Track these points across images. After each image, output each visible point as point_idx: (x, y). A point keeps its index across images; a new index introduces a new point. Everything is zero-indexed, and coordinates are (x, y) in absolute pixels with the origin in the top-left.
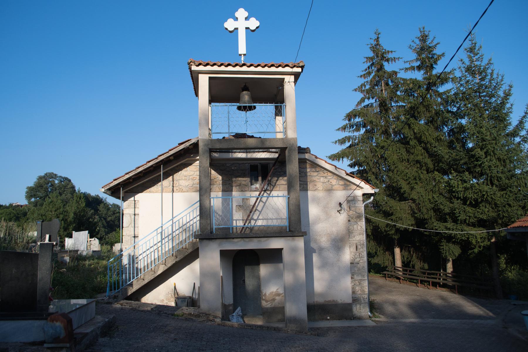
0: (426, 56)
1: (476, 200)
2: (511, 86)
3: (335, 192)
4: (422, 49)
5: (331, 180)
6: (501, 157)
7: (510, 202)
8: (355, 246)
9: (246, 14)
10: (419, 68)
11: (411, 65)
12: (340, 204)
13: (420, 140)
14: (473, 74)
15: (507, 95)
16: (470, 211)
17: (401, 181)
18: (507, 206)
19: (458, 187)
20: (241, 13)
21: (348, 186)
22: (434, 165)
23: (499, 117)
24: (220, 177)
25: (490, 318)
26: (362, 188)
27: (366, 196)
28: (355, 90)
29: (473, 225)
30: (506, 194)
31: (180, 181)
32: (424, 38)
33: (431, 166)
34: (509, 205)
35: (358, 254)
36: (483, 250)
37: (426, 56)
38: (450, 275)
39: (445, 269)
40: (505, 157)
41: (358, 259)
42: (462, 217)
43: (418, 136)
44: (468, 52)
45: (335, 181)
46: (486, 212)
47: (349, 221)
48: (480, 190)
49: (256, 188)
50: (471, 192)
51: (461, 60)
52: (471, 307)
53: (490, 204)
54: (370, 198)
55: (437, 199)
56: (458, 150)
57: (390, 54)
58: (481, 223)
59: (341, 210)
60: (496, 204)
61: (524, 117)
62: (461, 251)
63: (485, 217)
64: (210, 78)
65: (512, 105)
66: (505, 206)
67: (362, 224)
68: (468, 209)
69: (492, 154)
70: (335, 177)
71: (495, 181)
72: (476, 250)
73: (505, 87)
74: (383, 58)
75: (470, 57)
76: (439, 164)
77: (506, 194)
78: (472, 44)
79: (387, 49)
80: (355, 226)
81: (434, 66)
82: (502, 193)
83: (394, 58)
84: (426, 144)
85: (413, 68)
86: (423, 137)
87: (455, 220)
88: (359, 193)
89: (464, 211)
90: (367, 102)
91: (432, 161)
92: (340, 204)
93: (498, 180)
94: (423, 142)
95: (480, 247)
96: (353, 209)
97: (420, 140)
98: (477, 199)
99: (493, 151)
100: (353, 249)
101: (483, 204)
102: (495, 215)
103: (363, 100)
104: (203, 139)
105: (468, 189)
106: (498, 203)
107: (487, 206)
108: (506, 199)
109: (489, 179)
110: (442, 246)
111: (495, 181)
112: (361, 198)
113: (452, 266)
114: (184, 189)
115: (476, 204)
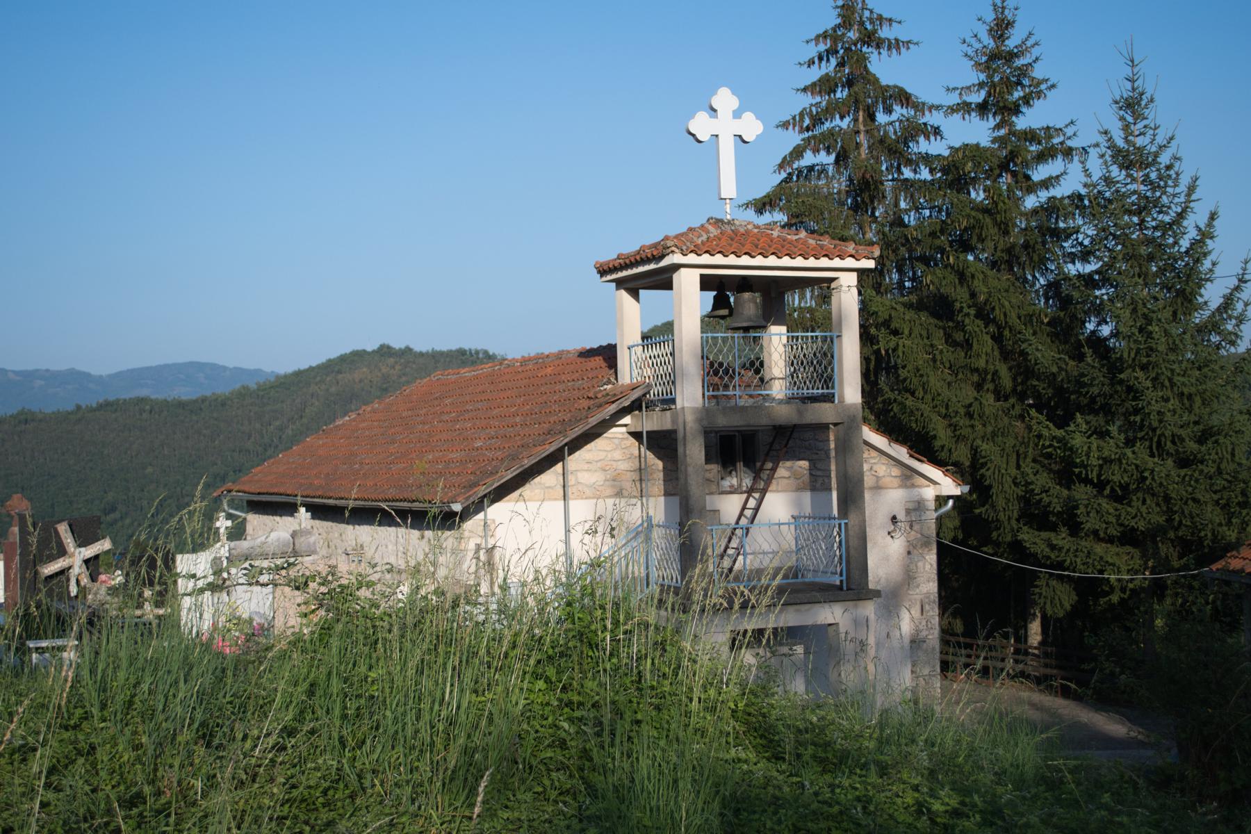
0: (1004, 80)
1: (1124, 487)
2: (1213, 216)
3: (883, 492)
4: (993, 57)
5: (875, 468)
6: (1186, 391)
7: (1199, 496)
8: (918, 607)
9: (734, 103)
10: (983, 108)
11: (965, 98)
12: (894, 519)
13: (983, 314)
14: (1127, 165)
15: (1205, 234)
16: (1111, 511)
17: (935, 418)
18: (1190, 502)
19: (1088, 455)
20: (725, 100)
21: (908, 478)
22: (1014, 379)
23: (1184, 282)
24: (660, 464)
25: (1141, 744)
26: (935, 483)
27: (941, 500)
28: (785, 125)
29: (1110, 540)
30: (1192, 476)
31: (579, 474)
32: (1001, 27)
33: (1007, 382)
34: (1195, 500)
35: (924, 623)
36: (1130, 598)
37: (1004, 80)
38: (1036, 652)
39: (1022, 638)
40: (1193, 390)
41: (924, 633)
42: (1091, 523)
43: (972, 290)
44: (1121, 108)
45: (884, 468)
46: (1144, 514)
47: (909, 553)
48: (1137, 466)
49: (732, 486)
50: (1117, 468)
51: (1106, 133)
52: (1113, 726)
53: (1153, 495)
54: (946, 503)
55: (1031, 478)
56: (1088, 365)
57: (886, 27)
58: (1129, 537)
59: (894, 531)
60: (1167, 499)
61: (1237, 288)
62: (1076, 598)
63: (1142, 525)
64: (702, 276)
65: (1214, 264)
66: (1186, 503)
67: (931, 558)
68: (1106, 505)
69: (1167, 383)
70: (884, 459)
71: (1169, 443)
72: (1115, 598)
73: (1185, 181)
74: (869, 38)
75: (1126, 128)
76: (1027, 379)
77: (1192, 476)
78: (1134, 90)
79: (877, 11)
80: (920, 564)
81: (1024, 109)
82: (1183, 472)
83: (897, 40)
84: (999, 327)
85: (964, 108)
86: (997, 311)
87: (1075, 529)
88: (929, 493)
89: (1098, 512)
90: (809, 159)
91: (1010, 369)
92: (894, 519)
93: (1173, 442)
94: (994, 321)
95: (1123, 590)
96: (916, 527)
97: (983, 314)
98: (1128, 485)
99: (1170, 380)
100: (916, 612)
101: (1140, 495)
102: (1162, 520)
103: (798, 153)
104: (694, 408)
105: (1111, 461)
106: (1173, 495)
107: (1148, 502)
108: (1190, 489)
109: (1155, 439)
110: (1037, 586)
111: (1169, 443)
112: (932, 505)
113: (1039, 630)
114: (588, 492)
115: (1121, 496)
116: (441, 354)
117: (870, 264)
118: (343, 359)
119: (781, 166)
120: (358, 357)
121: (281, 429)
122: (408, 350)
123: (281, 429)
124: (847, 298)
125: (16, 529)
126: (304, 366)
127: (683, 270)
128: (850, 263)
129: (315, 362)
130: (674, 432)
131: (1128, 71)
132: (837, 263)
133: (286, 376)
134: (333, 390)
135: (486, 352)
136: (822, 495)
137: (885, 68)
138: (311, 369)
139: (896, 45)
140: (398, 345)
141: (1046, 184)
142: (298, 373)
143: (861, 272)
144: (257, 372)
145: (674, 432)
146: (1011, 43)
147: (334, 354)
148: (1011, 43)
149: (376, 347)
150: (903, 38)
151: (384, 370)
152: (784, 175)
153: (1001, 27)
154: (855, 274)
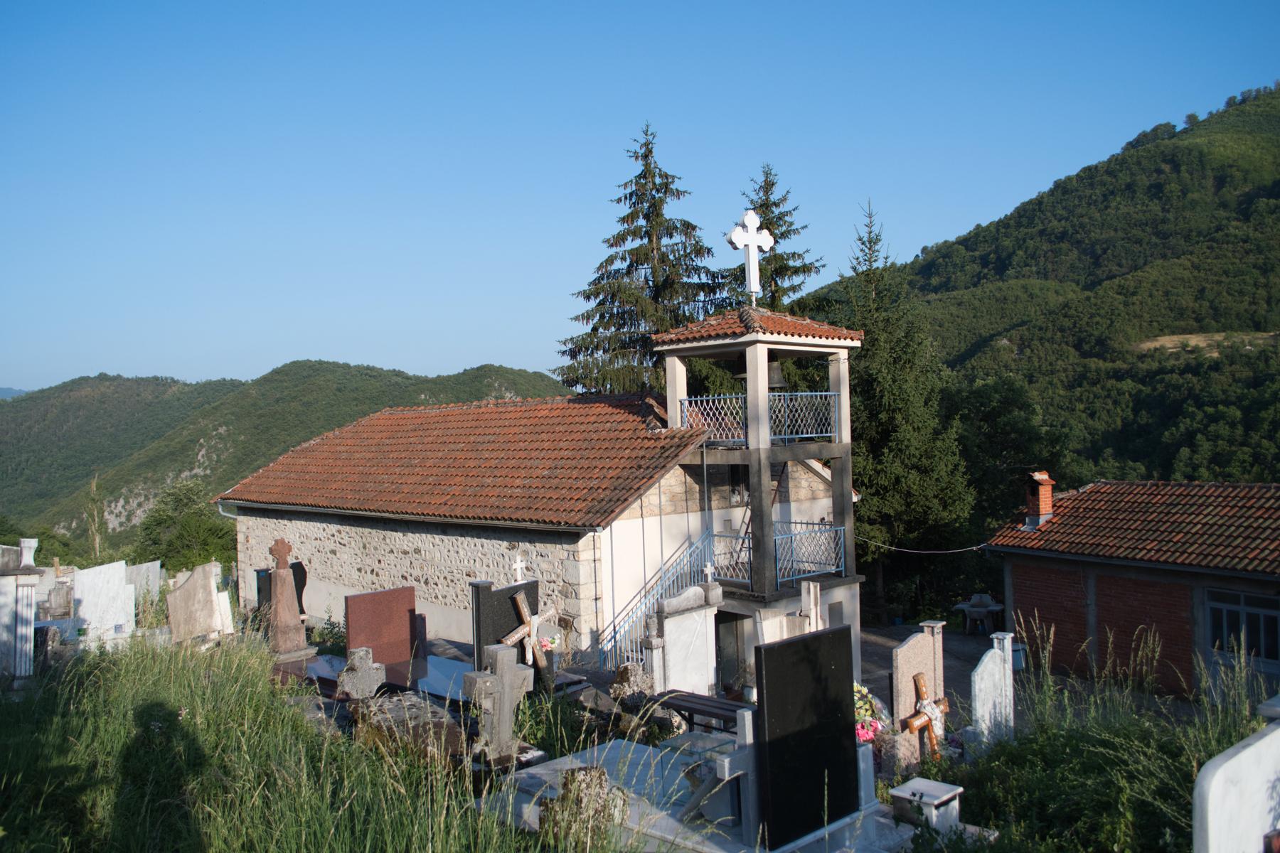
32: (768, 186)
116: (142, 379)
117: (857, 344)
118: (73, 382)
119: (599, 269)
120: (84, 380)
121: (30, 428)
122: (119, 377)
123: (30, 428)
124: (841, 368)
125: (755, 691)
126: (46, 386)
127: (759, 345)
128: (842, 343)
129: (55, 382)
130: (746, 467)
131: (868, 220)
132: (836, 342)
133: (34, 393)
134: (67, 402)
135: (172, 379)
136: (785, 505)
137: (672, 210)
138: (51, 389)
139: (678, 194)
140: (112, 373)
141: (794, 289)
142: (42, 391)
143: (850, 349)
144: (10, 389)
145: (746, 467)
146: (774, 197)
147: (67, 379)
148: (774, 197)
149: (96, 374)
150: (681, 189)
151: (103, 389)
152: (597, 275)
153: (768, 186)
154: (846, 351)
